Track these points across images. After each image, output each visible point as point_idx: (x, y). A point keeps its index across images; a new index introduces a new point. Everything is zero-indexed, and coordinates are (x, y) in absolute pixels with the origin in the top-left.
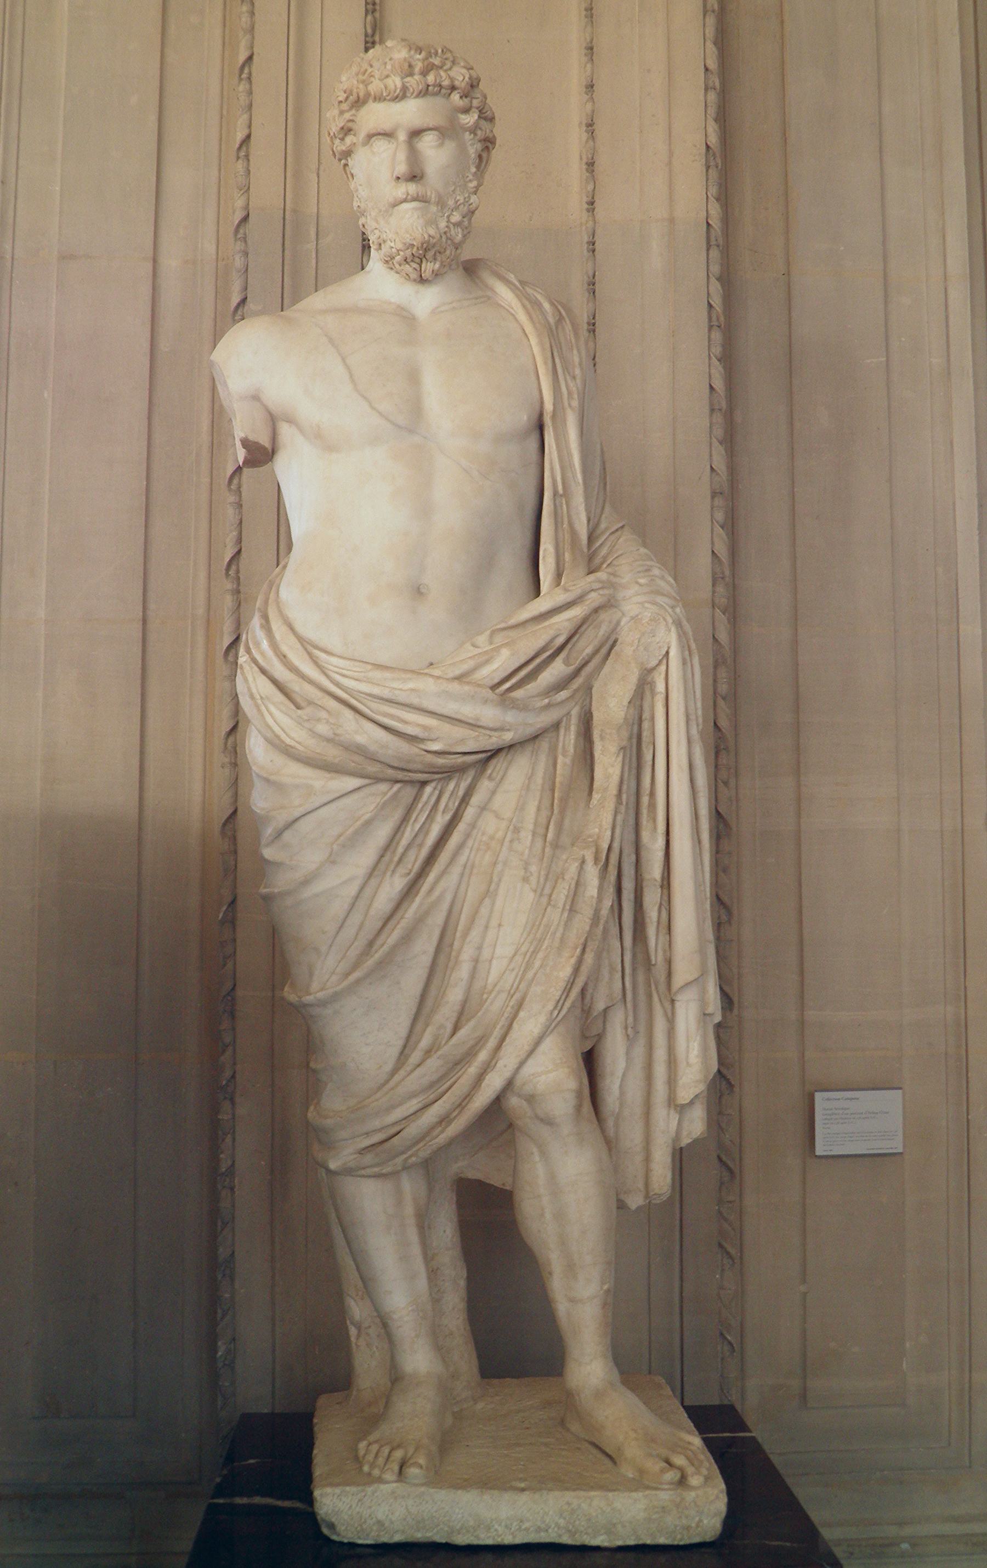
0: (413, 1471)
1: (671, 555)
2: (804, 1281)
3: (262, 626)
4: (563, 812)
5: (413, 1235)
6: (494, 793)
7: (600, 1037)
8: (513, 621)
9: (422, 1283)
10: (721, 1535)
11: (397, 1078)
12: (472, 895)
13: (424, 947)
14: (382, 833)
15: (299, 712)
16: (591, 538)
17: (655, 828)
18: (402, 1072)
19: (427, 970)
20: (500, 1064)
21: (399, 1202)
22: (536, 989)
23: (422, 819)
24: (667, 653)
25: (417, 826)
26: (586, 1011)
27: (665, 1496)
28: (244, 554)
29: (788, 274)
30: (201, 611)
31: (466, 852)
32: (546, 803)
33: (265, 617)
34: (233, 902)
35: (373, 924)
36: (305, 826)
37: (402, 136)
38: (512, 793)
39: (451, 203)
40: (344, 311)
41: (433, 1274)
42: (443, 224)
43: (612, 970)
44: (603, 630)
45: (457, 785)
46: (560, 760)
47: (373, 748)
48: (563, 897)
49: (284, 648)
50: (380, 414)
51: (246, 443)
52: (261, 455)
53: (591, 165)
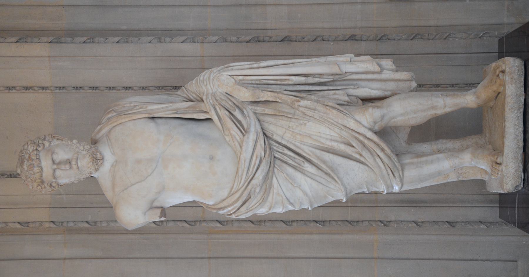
0: (499, 161)
4: (284, 112)
5: (423, 159)
6: (277, 135)
7: (358, 97)
8: (221, 128)
9: (441, 156)
11: (369, 165)
12: (310, 141)
13: (328, 157)
14: (290, 170)
15: (252, 197)
16: (191, 101)
17: (289, 80)
18: (368, 163)
20: (364, 133)
21: (412, 163)
25: (288, 159)
26: (348, 104)
27: (507, 78)
30: (206, 236)
32: (280, 118)
33: (220, 209)
34: (316, 222)
35: (320, 173)
36: (288, 195)
37: (55, 167)
38: (279, 130)
39: (77, 150)
40: (114, 185)
41: (439, 151)
42: (85, 152)
43: (335, 94)
46: (266, 112)
47: (264, 174)
49: (231, 202)
51: (160, 217)
52: (164, 211)
53: (27, 88)
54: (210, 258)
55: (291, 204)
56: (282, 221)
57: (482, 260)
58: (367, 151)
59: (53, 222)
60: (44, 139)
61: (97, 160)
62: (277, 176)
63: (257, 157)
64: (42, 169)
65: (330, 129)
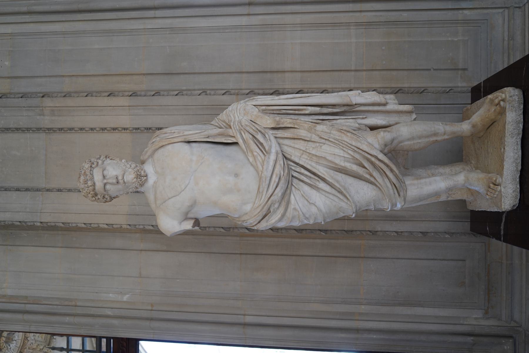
1: (223, 107)
2: (430, 70)
5: (423, 181)
7: (366, 126)
10: (521, 89)
11: (378, 185)
13: (340, 177)
14: (306, 188)
17: (305, 109)
18: (377, 183)
20: (376, 154)
28: (223, 226)
30: (238, 238)
34: (320, 230)
39: (124, 167)
42: (130, 170)
47: (282, 191)
52: (197, 222)
54: (241, 254)
57: (440, 260)
58: (377, 172)
60: (99, 158)
62: (294, 193)
63: (276, 176)
64: (94, 183)
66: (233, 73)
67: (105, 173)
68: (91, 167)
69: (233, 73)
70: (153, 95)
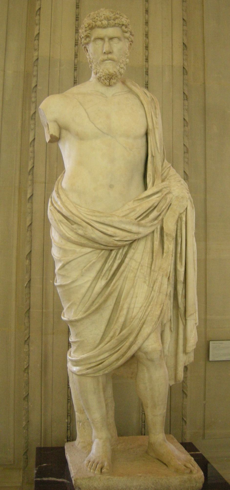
2: (205, 400)
3: (58, 197)
5: (102, 394)
6: (134, 253)
8: (140, 197)
12: (127, 287)
13: (111, 303)
14: (98, 266)
17: (182, 264)
19: (111, 311)
20: (137, 342)
22: (149, 318)
23: (111, 262)
24: (186, 208)
25: (110, 264)
28: (35, 168)
29: (204, 83)
30: (17, 185)
31: (125, 273)
34: (30, 281)
38: (139, 255)
39: (121, 61)
42: (118, 68)
44: (168, 200)
45: (123, 251)
48: (157, 288)
50: (98, 128)
52: (55, 140)
55: (63, 266)
56: (31, 251)
59: (37, 59)
61: (109, 80)
65: (141, 308)
66: (206, 183)
67: (116, 40)
68: (123, 25)
69: (206, 183)
70: (184, 93)
